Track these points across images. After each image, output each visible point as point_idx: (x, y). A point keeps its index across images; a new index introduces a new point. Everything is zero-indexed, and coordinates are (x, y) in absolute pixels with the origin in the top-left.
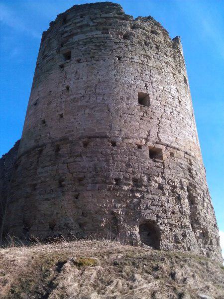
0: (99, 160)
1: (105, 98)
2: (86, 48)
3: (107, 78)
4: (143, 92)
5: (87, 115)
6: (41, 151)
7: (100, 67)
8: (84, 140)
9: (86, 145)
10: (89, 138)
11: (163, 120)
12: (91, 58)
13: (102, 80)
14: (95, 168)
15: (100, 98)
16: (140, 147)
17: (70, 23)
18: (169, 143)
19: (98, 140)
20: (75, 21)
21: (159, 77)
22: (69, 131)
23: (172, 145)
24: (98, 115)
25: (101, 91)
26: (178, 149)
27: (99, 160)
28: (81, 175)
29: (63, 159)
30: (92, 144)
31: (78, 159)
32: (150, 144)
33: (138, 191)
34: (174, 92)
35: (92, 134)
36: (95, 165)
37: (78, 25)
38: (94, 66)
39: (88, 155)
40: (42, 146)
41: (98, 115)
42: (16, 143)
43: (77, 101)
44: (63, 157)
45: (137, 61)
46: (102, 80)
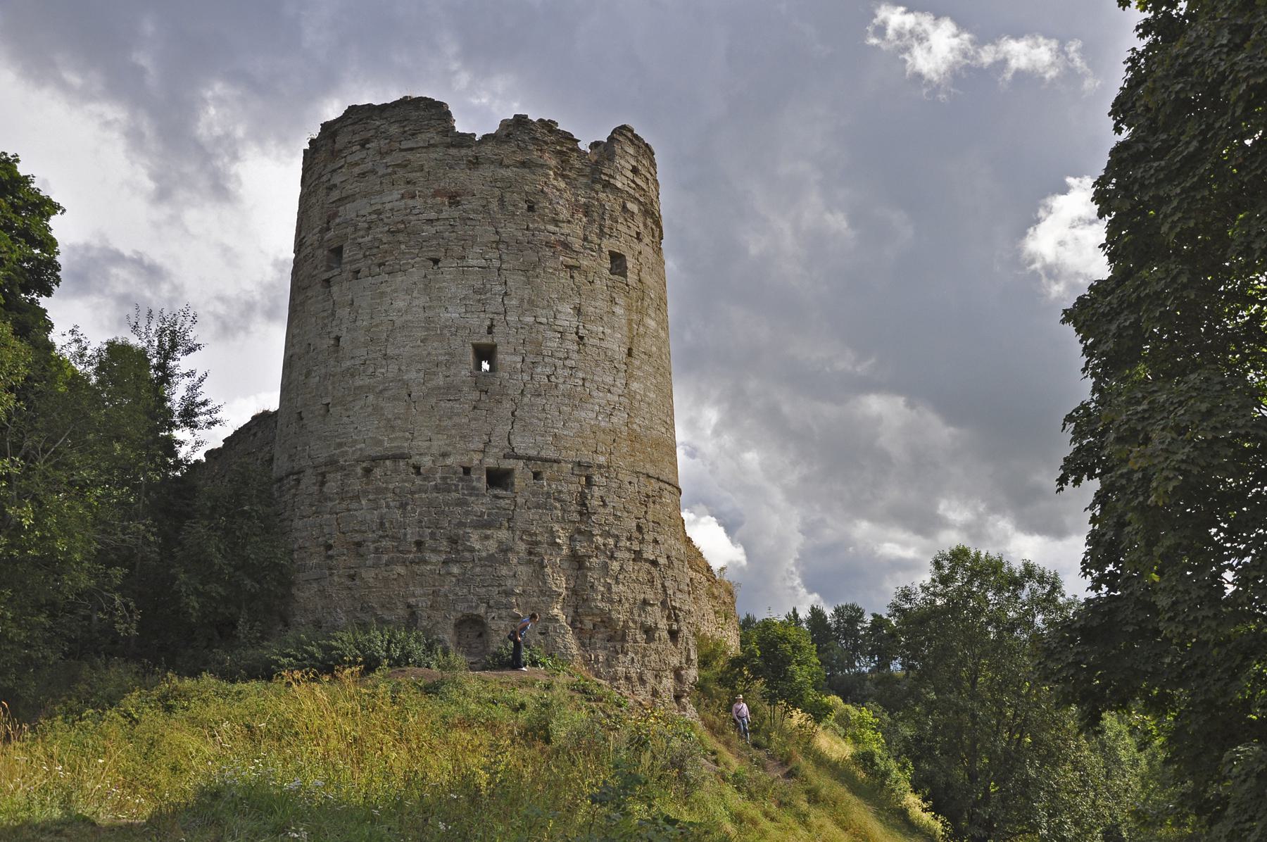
0: (388, 506)
1: (403, 368)
2: (370, 238)
3: (409, 317)
4: (484, 341)
5: (370, 409)
6: (298, 481)
7: (395, 291)
8: (364, 465)
9: (368, 471)
10: (374, 459)
11: (526, 400)
12: (380, 265)
13: (398, 323)
14: (382, 524)
15: (393, 367)
16: (467, 471)
17: (342, 162)
18: (533, 453)
19: (388, 462)
20: (349, 159)
21: (526, 293)
22: (340, 445)
23: (543, 454)
24: (389, 409)
25: (397, 352)
26: (557, 461)
27: (388, 506)
28: (358, 537)
29: (330, 504)
30: (378, 472)
31: (354, 505)
32: (491, 462)
33: (456, 561)
34: (567, 318)
35: (375, 451)
36: (382, 517)
37: (357, 170)
38: (384, 288)
39: (371, 497)
40: (298, 473)
41: (389, 409)
42: (254, 418)
43: (353, 375)
44: (331, 500)
45: (474, 262)
46: (398, 323)
